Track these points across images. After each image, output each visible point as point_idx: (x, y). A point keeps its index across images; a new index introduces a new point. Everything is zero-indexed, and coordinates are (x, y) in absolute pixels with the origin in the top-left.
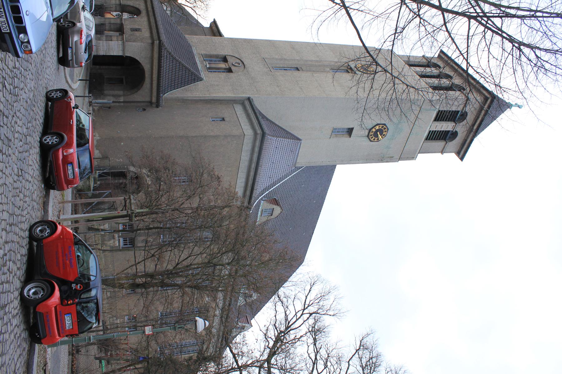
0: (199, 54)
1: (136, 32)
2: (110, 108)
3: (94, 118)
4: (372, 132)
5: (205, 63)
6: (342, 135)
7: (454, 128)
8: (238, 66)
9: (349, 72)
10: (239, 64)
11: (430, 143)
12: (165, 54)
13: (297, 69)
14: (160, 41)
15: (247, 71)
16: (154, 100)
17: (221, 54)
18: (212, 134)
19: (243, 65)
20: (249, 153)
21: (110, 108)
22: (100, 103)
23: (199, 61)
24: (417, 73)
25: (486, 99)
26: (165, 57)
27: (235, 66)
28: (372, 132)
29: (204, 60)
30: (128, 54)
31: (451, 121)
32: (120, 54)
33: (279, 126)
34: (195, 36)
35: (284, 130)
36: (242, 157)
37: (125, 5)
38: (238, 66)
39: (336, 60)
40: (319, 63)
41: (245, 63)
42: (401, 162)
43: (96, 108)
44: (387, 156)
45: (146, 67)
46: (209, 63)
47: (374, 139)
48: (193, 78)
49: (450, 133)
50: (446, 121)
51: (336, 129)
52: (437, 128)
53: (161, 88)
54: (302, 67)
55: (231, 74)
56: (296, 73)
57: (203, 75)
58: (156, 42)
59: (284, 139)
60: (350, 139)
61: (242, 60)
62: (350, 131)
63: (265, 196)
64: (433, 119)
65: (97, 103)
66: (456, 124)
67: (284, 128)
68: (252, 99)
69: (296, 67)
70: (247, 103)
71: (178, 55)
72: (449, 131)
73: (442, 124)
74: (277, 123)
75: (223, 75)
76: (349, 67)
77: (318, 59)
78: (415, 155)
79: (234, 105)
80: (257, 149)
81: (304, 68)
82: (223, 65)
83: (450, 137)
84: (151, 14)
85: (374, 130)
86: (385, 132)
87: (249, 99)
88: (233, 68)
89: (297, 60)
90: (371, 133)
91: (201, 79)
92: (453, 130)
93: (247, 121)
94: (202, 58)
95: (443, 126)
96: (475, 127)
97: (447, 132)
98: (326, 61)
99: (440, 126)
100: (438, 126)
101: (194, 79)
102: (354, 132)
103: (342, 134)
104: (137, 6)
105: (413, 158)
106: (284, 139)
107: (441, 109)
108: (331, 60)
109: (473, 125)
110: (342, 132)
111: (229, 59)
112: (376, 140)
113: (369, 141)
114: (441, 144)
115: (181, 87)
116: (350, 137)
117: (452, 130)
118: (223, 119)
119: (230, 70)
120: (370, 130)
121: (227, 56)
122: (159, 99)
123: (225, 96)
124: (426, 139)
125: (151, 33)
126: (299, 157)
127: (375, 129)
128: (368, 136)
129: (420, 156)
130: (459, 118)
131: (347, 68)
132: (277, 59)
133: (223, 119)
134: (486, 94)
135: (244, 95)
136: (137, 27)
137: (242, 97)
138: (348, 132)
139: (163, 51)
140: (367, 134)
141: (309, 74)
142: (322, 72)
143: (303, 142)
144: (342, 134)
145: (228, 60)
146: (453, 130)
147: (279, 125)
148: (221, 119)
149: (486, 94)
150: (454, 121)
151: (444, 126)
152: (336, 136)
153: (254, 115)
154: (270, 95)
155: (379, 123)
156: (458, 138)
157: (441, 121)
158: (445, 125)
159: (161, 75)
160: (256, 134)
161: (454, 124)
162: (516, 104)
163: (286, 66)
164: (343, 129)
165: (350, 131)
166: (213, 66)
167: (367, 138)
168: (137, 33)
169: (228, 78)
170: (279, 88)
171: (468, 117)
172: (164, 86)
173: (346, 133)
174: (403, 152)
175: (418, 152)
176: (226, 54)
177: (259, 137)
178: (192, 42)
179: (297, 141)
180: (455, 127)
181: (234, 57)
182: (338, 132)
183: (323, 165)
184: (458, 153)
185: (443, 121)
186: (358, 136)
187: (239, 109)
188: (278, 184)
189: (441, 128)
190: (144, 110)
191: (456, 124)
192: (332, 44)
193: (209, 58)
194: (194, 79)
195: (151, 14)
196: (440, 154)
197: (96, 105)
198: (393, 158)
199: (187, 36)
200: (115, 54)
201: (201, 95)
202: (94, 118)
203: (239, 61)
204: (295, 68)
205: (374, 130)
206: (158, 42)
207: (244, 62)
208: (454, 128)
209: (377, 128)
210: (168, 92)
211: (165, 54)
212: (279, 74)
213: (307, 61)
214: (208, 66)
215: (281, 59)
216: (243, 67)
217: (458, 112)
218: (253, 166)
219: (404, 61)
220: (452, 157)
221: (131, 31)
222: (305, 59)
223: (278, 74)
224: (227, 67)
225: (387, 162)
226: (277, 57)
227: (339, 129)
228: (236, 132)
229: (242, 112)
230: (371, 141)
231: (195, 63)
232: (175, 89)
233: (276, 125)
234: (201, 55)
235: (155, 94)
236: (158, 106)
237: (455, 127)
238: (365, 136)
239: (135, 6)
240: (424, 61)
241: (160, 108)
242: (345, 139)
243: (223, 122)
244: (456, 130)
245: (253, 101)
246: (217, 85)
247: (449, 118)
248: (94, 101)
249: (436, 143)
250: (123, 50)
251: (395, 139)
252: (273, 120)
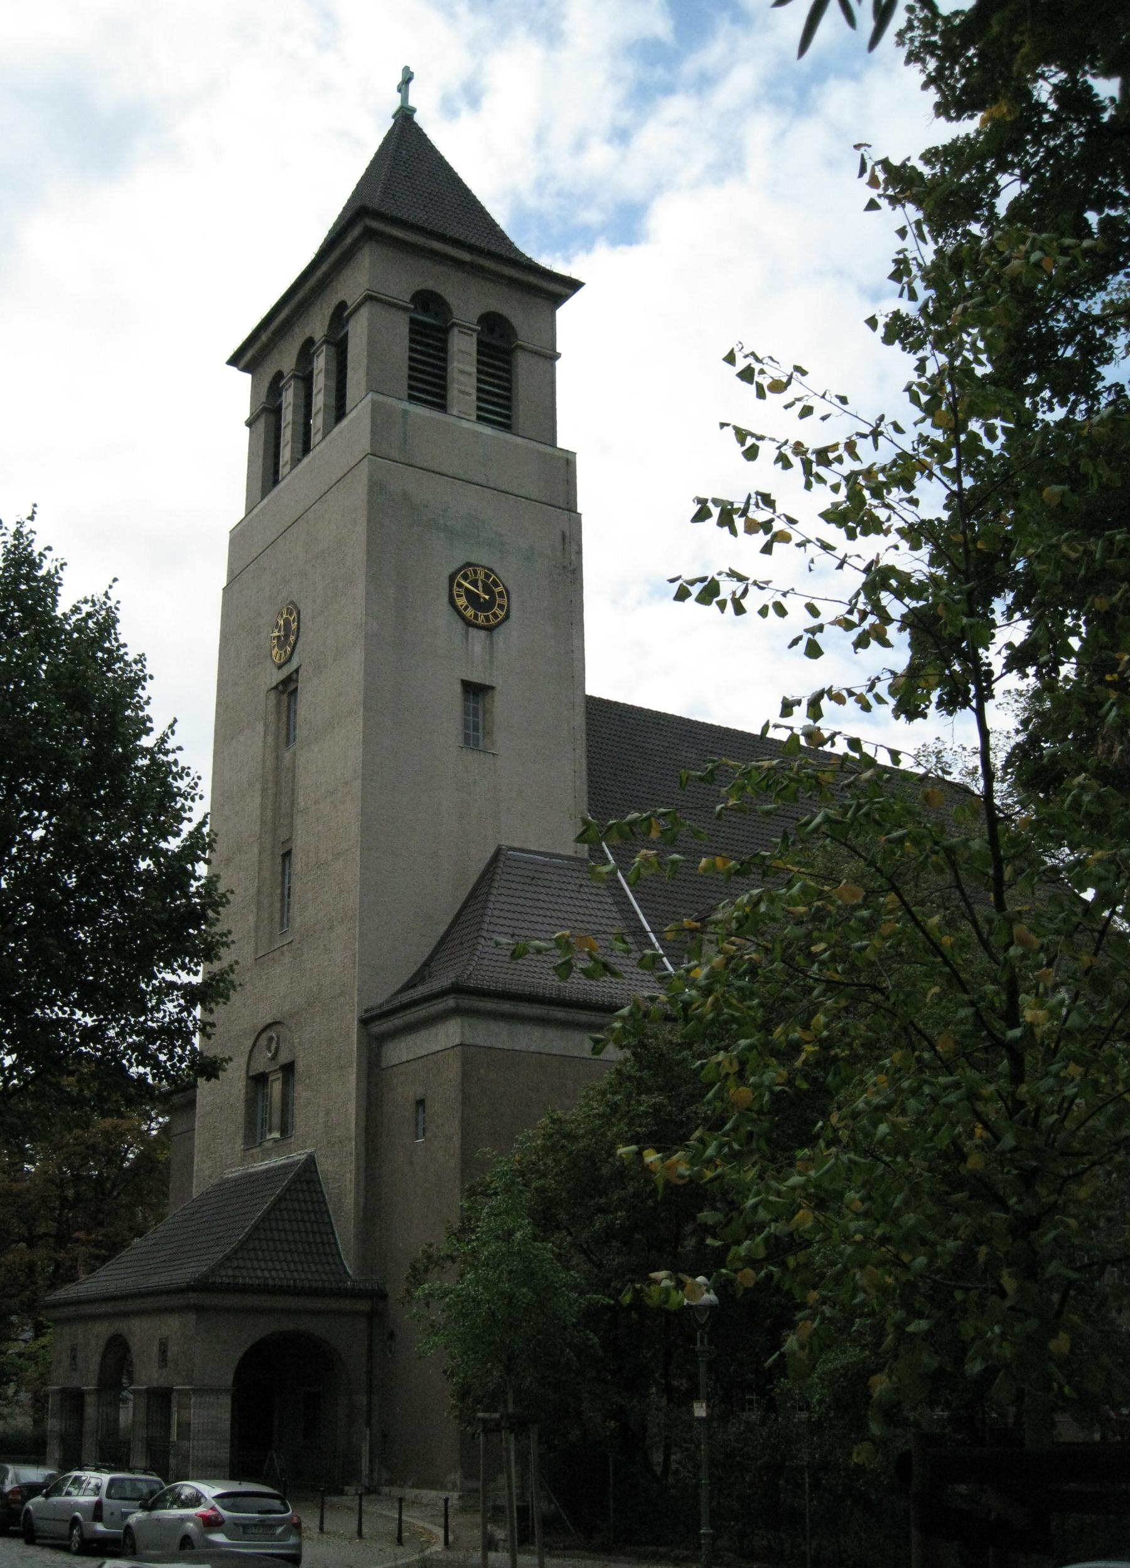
0: (243, 1159)
1: (169, 1354)
2: (385, 1436)
3: (410, 1483)
4: (476, 616)
5: (268, 1145)
6: (487, 716)
7: (469, 329)
8: (278, 1043)
9: (296, 689)
10: (271, 1039)
11: (521, 407)
12: (230, 1272)
13: (287, 855)
14: (190, 1288)
15: (291, 1016)
16: (363, 1306)
17: (243, 1091)
18: (457, 1141)
19: (274, 1027)
20: (522, 1029)
21: (385, 1436)
22: (371, 1461)
23: (263, 1160)
24: (295, 462)
25: (370, 235)
26: (237, 1273)
27: (277, 1049)
28: (476, 616)
29: (260, 1144)
30: (228, 1379)
31: (445, 341)
32: (227, 1400)
33: (452, 925)
34: (195, 1167)
35: (464, 907)
36: (532, 1049)
37: (100, 1379)
38: (278, 1043)
39: (260, 727)
40: (270, 785)
41: (269, 1021)
42: (583, 505)
43: (385, 1475)
44: (559, 554)
45: (264, 1327)
46: (270, 1132)
47: (501, 607)
48: (305, 1188)
49: (487, 340)
50: (444, 360)
51: (467, 738)
52: (467, 389)
53: (327, 1285)
54: (282, 839)
55: (300, 1067)
56: (298, 863)
57: (299, 1156)
58: (193, 1298)
59: (487, 919)
60: (499, 688)
61: (260, 1027)
62: (474, 691)
63: (674, 959)
64: (436, 414)
65: (372, 1471)
66: (454, 324)
67: (458, 906)
68: (366, 1011)
69: (279, 860)
70: (377, 1028)
71: (236, 1232)
72: (480, 343)
73: (456, 375)
74: (443, 929)
75: (301, 1093)
76: (280, 687)
77: (258, 786)
78: (559, 458)
79: (383, 1065)
80: (506, 1007)
81: (283, 835)
82: (276, 1088)
83: (502, 336)
84: (121, 1306)
85: (470, 613)
86: (475, 572)
87: (365, 1022)
88: (283, 1058)
89: (260, 852)
90: (481, 620)
91: (311, 1160)
92: (473, 330)
93: (427, 1032)
94: (254, 1151)
95: (462, 372)
96: (467, 257)
97: (483, 347)
98: (264, 761)
99: (462, 378)
100: (463, 388)
101: (308, 1182)
102: (476, 677)
103: (484, 714)
104: (102, 1342)
105: (568, 461)
106: (487, 919)
107: (404, 391)
108: (261, 744)
109: (459, 264)
110: (476, 715)
111: (260, 1066)
112: (505, 602)
113: (507, 623)
114: (523, 364)
115: (331, 1222)
116: (492, 688)
117: (475, 335)
118: (420, 1103)
119: (289, 1069)
120: (469, 623)
121: (251, 1074)
122: (361, 1290)
123: (354, 1095)
124: (507, 427)
125: (171, 1310)
126: (558, 851)
127: (466, 608)
128: (490, 629)
129: (562, 442)
130: (437, 315)
131: (283, 692)
132: (258, 916)
133: (420, 1103)
134: (356, 232)
135: (355, 1038)
136: (155, 1349)
137: (359, 1042)
138: (476, 695)
139: (218, 1280)
140: (483, 633)
141: (299, 821)
142: (294, 776)
143: (505, 843)
144: (484, 714)
145: (261, 1070)
146: (473, 330)
147: (449, 921)
148: (421, 1109)
149: (356, 232)
150: (446, 330)
151: (461, 366)
152: (489, 733)
153: (408, 1012)
154: (354, 955)
155: (445, 599)
156: (505, 310)
157: (444, 378)
158: (459, 361)
159: (289, 1287)
160: (457, 1012)
161: (456, 330)
162: (399, 90)
163: (279, 891)
164: (466, 712)
165: (474, 691)
166: (276, 1119)
167: (495, 633)
168: (173, 1350)
169: (309, 1077)
170: (335, 923)
171: (430, 285)
172: (324, 1277)
173: (480, 701)
174: (544, 500)
175: (549, 449)
176: (243, 1074)
177: (467, 1002)
178: (210, 1177)
179: (501, 865)
180: (465, 330)
181: (251, 1051)
182: (476, 729)
183: (584, 767)
184: (558, 300)
185: (445, 369)
186: (491, 662)
187: (399, 1052)
188: (642, 917)
189: (469, 374)
190: (392, 1335)
191: (454, 324)
192: (216, 730)
193: (253, 1133)
194: (308, 1182)
195: (121, 1306)
196: (558, 363)
197: (375, 1475)
198: (567, 534)
199: (194, 1190)
200: (228, 1415)
201: (353, 1167)
202: (410, 1483)
203: (265, 1036)
204: (284, 861)
205: (470, 613)
206: (191, 1295)
207: (265, 1024)
208: (469, 329)
209: (462, 602)
210: (343, 1264)
211: (230, 1272)
212: (299, 919)
213: (263, 822)
214: (276, 1135)
215: (259, 905)
216: (278, 1028)
217: (412, 321)
218: (559, 1014)
219: (262, 499)
220: (566, 315)
221: (166, 1365)
222: (257, 828)
223: (298, 920)
224: (280, 1075)
225: (579, 552)
226: (252, 918)
227: (466, 726)
228: (453, 1070)
229: (403, 1044)
230: (507, 616)
231: (269, 1175)
232: (336, 1244)
233: (447, 933)
234: (247, 1153)
235: (346, 1304)
236: (383, 1296)
237: (464, 327)
238: (491, 643)
239: (101, 1350)
240: (261, 424)
241: (388, 1287)
242: (501, 705)
243: (428, 1103)
244: (408, 298)
245: (373, 1009)
246: (327, 1114)
247: (435, 348)
248: (365, 1481)
249: (520, 383)
250: (215, 1391)
251: (501, 535)
252: (434, 943)
